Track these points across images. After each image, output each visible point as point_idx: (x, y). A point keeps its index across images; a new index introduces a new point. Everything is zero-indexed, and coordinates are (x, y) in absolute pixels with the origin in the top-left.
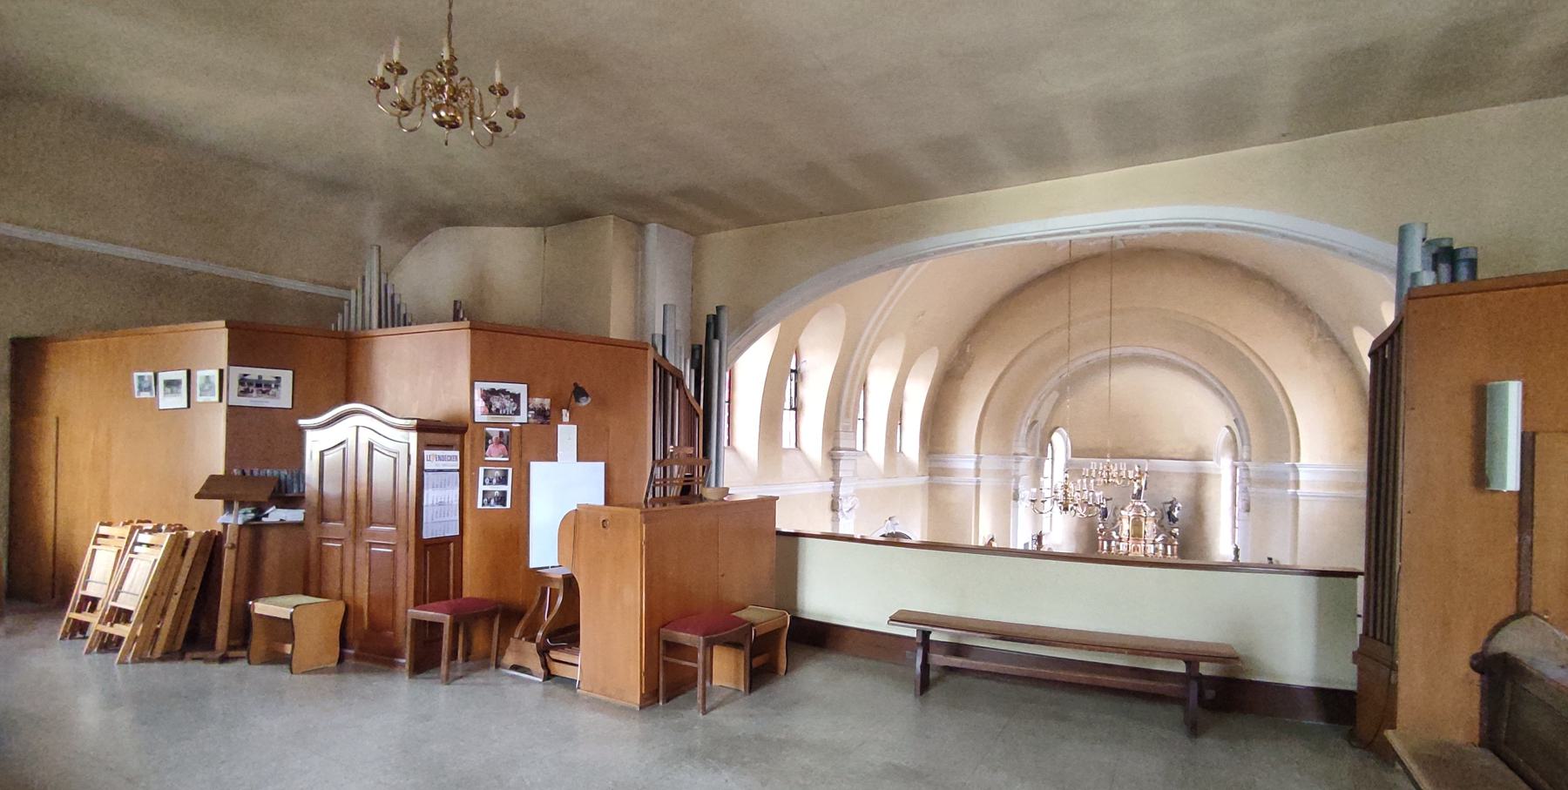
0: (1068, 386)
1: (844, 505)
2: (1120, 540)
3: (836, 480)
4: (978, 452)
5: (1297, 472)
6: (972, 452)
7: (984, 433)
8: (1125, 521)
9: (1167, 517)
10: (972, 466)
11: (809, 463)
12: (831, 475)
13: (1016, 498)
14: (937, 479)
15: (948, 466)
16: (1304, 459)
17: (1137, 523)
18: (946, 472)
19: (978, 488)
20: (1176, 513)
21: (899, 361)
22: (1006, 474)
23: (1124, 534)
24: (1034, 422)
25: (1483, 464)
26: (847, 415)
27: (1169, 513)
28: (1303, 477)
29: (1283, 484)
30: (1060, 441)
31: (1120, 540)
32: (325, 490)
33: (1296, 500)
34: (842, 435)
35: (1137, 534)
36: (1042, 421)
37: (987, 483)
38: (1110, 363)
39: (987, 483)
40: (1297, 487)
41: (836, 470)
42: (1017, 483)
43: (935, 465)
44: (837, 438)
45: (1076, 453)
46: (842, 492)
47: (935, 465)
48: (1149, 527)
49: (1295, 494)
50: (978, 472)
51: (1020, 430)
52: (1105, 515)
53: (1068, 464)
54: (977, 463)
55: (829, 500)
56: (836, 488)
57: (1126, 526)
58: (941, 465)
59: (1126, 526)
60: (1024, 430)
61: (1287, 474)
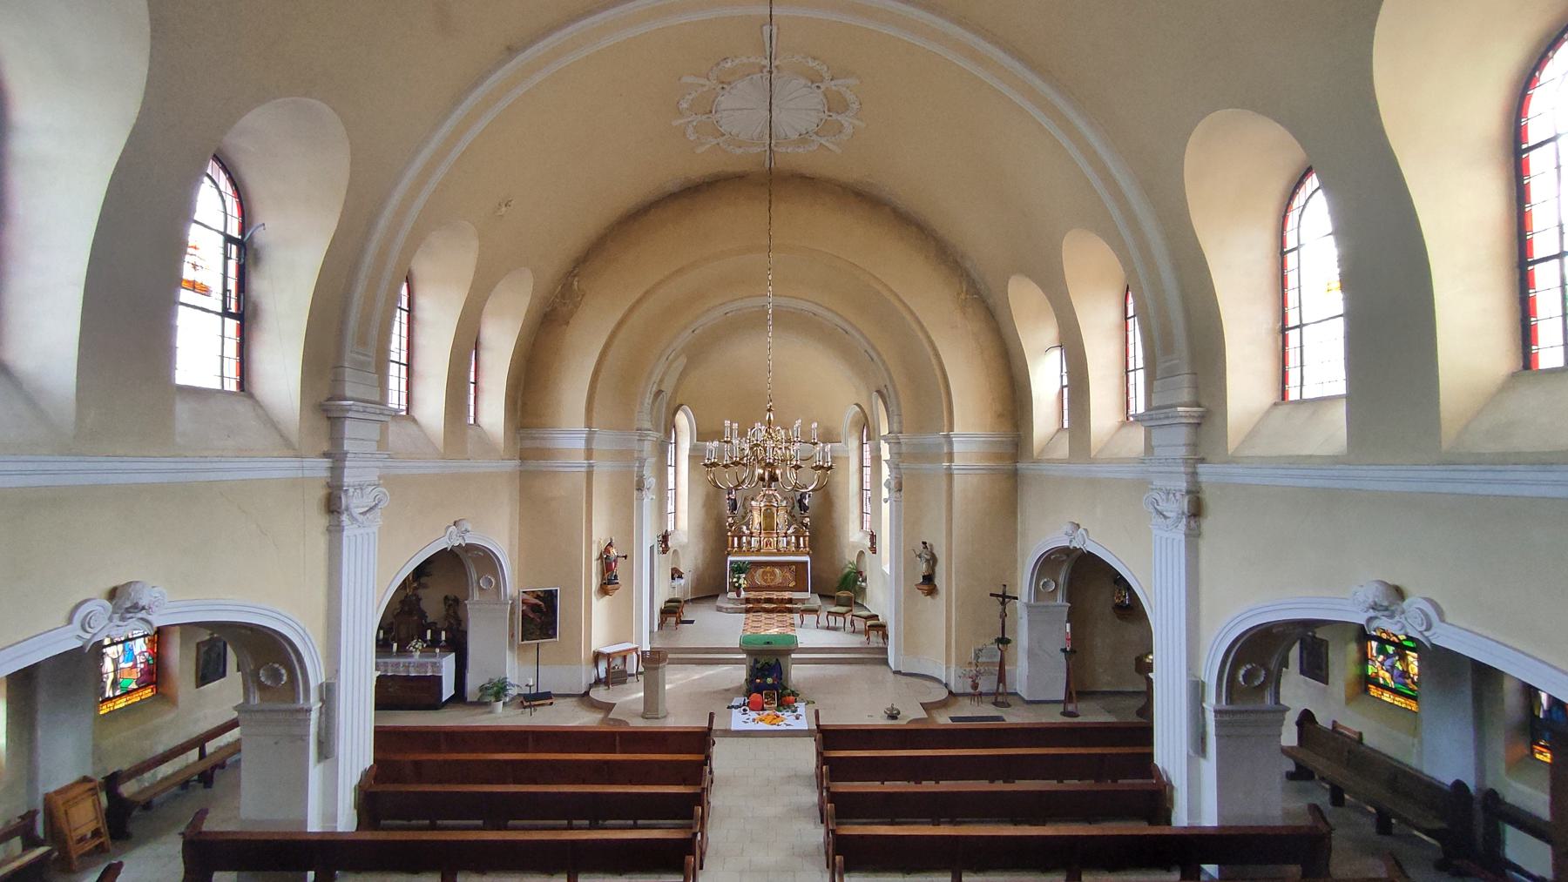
0: (697, 353)
1: (355, 502)
2: (751, 535)
3: (336, 457)
4: (589, 424)
5: (951, 443)
6: (580, 425)
7: (596, 405)
8: (756, 514)
9: (799, 504)
10: (581, 444)
11: (269, 421)
12: (325, 447)
13: (640, 489)
14: (532, 465)
15: (549, 445)
16: (956, 430)
17: (768, 515)
18: (545, 454)
19: (589, 474)
21: (469, 274)
22: (625, 455)
23: (755, 530)
24: (659, 392)
25: (329, 602)
26: (363, 341)
27: (800, 501)
28: (956, 448)
29: (937, 458)
30: (683, 420)
31: (751, 535)
32: (321, 542)
33: (950, 476)
34: (349, 373)
35: (768, 527)
36: (668, 387)
37: (603, 468)
38: (753, 322)
39: (603, 468)
40: (951, 459)
41: (336, 437)
42: (641, 467)
43: (528, 444)
44: (338, 380)
46: (349, 478)
47: (528, 444)
48: (781, 518)
49: (949, 468)
50: (589, 453)
51: (641, 398)
52: (734, 507)
53: (693, 449)
54: (589, 441)
55: (321, 493)
56: (337, 470)
57: (757, 519)
58: (537, 444)
59: (757, 519)
60: (648, 400)
61: (939, 445)
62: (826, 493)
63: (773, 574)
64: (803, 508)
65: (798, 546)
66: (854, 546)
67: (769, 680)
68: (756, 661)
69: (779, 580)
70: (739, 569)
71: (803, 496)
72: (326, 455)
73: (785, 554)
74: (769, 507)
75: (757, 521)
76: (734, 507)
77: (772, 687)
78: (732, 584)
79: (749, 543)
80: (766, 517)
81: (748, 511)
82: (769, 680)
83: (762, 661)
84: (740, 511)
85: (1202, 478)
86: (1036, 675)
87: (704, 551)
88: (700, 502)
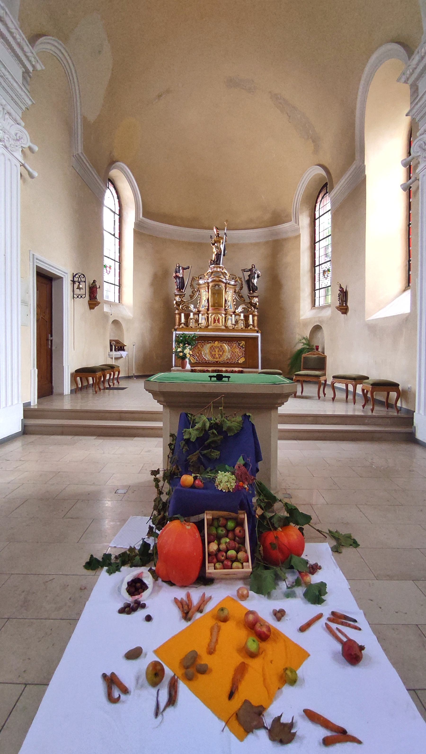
17: (217, 293)
20: (255, 281)
27: (249, 282)
35: (217, 304)
45: (148, 211)
48: (229, 296)
52: (181, 286)
57: (205, 295)
59: (205, 295)
62: (276, 282)
63: (221, 349)
64: (252, 288)
65: (247, 325)
66: (305, 324)
67: (225, 480)
68: (186, 422)
69: (227, 355)
70: (184, 341)
71: (251, 277)
72: (227, 547)
73: (234, 330)
74: (217, 283)
75: (204, 298)
76: (181, 286)
77: (237, 501)
78: (177, 353)
79: (197, 321)
80: (213, 294)
81: (196, 291)
82: (225, 480)
83: (203, 420)
84: (188, 291)
85: (249, 593)
86: (268, 575)
87: (152, 329)
88: (147, 279)
